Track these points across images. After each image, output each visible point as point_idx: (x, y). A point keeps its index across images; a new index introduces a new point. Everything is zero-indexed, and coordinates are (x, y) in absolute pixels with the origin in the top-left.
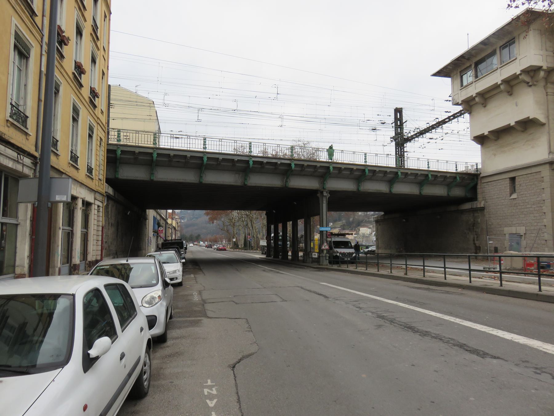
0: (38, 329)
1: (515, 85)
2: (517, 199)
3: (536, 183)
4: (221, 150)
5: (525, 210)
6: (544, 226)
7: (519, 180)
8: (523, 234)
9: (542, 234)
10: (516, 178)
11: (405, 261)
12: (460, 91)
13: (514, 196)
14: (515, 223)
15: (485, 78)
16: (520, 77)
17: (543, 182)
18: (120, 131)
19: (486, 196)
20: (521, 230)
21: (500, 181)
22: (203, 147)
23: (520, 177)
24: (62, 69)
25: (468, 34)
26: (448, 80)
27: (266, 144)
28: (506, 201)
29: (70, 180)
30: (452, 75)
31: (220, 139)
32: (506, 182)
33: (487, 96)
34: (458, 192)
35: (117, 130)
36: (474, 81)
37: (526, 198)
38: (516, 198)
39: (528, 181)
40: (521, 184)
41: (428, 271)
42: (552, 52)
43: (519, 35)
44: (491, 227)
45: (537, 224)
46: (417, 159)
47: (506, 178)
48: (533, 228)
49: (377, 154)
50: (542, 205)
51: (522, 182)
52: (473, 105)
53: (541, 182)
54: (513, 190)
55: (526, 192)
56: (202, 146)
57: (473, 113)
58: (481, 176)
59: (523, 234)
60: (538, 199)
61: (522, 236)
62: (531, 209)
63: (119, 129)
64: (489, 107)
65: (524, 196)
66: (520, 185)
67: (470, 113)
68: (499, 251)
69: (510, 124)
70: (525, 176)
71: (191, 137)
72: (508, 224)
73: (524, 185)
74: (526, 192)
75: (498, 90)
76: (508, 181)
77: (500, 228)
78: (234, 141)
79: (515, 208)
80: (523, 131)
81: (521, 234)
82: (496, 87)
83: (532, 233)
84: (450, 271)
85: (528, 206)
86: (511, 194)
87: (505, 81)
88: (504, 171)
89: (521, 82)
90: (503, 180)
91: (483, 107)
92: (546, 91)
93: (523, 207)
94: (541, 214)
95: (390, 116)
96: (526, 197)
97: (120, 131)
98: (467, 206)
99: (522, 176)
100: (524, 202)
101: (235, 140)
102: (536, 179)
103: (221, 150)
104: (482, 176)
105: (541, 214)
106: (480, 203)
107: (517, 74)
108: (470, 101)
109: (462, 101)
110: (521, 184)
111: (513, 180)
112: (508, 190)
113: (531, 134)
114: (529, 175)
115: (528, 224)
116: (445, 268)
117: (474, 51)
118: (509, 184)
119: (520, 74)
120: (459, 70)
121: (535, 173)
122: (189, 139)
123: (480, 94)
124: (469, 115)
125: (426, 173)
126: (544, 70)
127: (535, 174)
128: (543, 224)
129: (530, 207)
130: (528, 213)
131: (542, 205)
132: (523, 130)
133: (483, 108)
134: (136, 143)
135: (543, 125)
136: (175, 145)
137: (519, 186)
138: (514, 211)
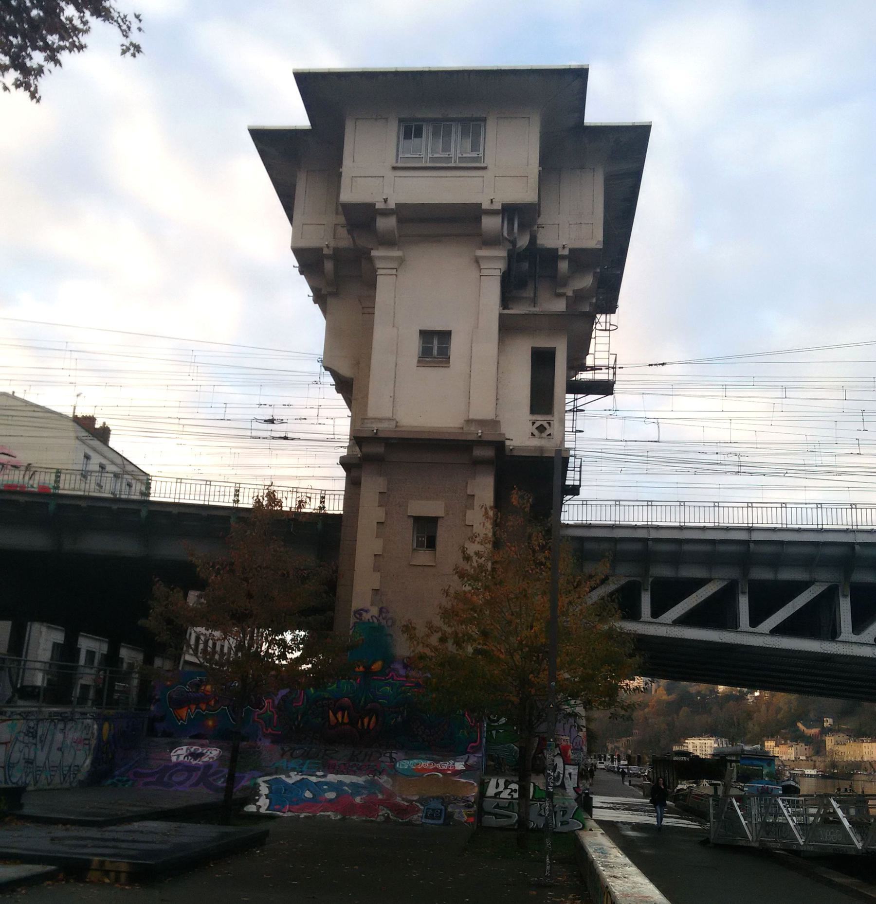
0: (395, 147)
4: (857, 525)
18: (60, 473)
22: (234, 500)
24: (824, 458)
27: (788, 505)
29: (37, 671)
31: (717, 502)
35: (55, 471)
42: (321, 361)
46: (175, 480)
49: (785, 503)
56: (232, 498)
63: (58, 469)
71: (788, 505)
78: (712, 504)
84: (468, 162)
95: (305, 419)
97: (60, 473)
101: (748, 503)
103: (857, 525)
122: (750, 509)
126: (328, 257)
134: (714, 523)
136: (211, 498)
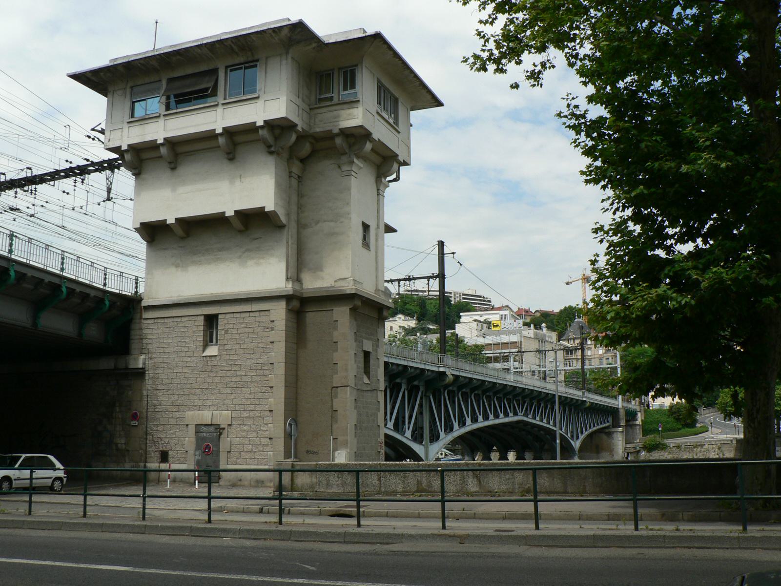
1: (181, 153)
2: (218, 358)
3: (258, 330)
5: (233, 379)
6: (268, 412)
7: (226, 322)
8: (226, 427)
9: (264, 426)
10: (220, 317)
11: (142, 488)
12: (126, 126)
13: (212, 351)
14: (210, 404)
15: (190, 114)
16: (260, 132)
17: (272, 329)
19: (150, 346)
20: (222, 417)
21: (183, 319)
23: (228, 316)
25: (157, 22)
26: (101, 101)
28: (193, 359)
30: (111, 89)
32: (197, 323)
33: (180, 149)
34: (93, 332)
36: (163, 114)
37: (236, 357)
38: (216, 356)
39: (243, 326)
40: (228, 330)
41: (220, 510)
43: (267, 58)
44: (156, 410)
45: (255, 407)
47: (197, 315)
48: (245, 414)
50: (267, 372)
51: (231, 325)
52: (181, 153)
53: (268, 330)
54: (209, 339)
55: (237, 347)
57: (142, 176)
58: (144, 303)
59: (226, 427)
60: (261, 361)
61: (224, 429)
62: (244, 378)
64: (182, 170)
65: (233, 352)
66: (227, 331)
67: (137, 174)
68: (170, 460)
69: (224, 212)
70: (238, 315)
72: (195, 406)
73: (234, 331)
74: (237, 347)
75: (212, 144)
76: (201, 321)
77: (177, 413)
79: (212, 375)
80: (240, 232)
81: (221, 427)
82: (209, 137)
83: (243, 424)
85: (239, 373)
86: (205, 346)
87: (229, 132)
88: (195, 301)
89: (260, 140)
90: (191, 318)
91: (169, 167)
92: (289, 169)
93: (229, 374)
94: (264, 389)
96: (237, 356)
98: (106, 364)
99: (232, 315)
100: (231, 365)
102: (259, 322)
104: (146, 304)
105: (264, 389)
106: (140, 362)
107: (217, 132)
108: (235, 132)
109: (129, 145)
110: (228, 330)
111: (211, 321)
112: (201, 339)
113: (256, 239)
114: (247, 315)
115: (237, 408)
116: (209, 498)
117: (178, 57)
118: (202, 328)
119: (261, 127)
120: (130, 84)
121: (258, 313)
123: (172, 143)
124: (134, 177)
125: (56, 281)
126: (297, 132)
127: (257, 314)
128: (267, 407)
129: (244, 374)
130: (238, 386)
131: (267, 372)
132: (243, 228)
133: (170, 169)
135: (281, 227)
137: (223, 332)
138: (209, 381)
